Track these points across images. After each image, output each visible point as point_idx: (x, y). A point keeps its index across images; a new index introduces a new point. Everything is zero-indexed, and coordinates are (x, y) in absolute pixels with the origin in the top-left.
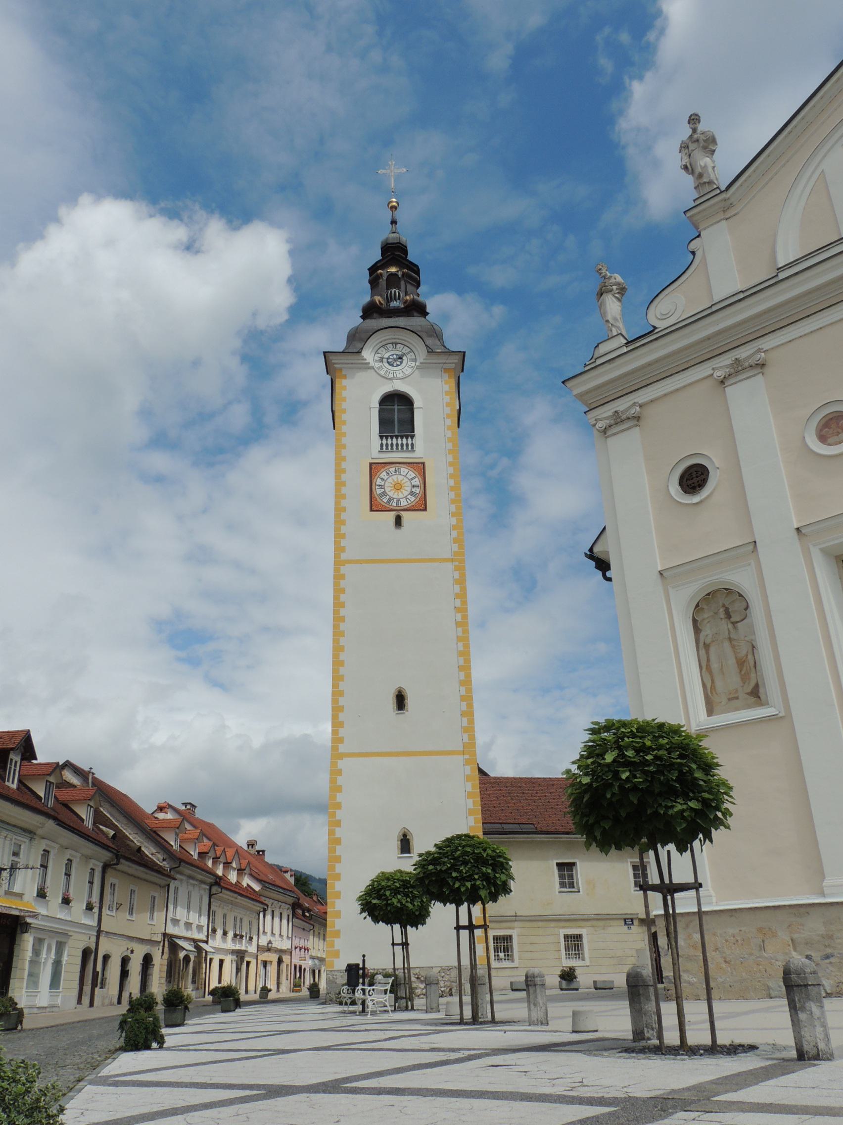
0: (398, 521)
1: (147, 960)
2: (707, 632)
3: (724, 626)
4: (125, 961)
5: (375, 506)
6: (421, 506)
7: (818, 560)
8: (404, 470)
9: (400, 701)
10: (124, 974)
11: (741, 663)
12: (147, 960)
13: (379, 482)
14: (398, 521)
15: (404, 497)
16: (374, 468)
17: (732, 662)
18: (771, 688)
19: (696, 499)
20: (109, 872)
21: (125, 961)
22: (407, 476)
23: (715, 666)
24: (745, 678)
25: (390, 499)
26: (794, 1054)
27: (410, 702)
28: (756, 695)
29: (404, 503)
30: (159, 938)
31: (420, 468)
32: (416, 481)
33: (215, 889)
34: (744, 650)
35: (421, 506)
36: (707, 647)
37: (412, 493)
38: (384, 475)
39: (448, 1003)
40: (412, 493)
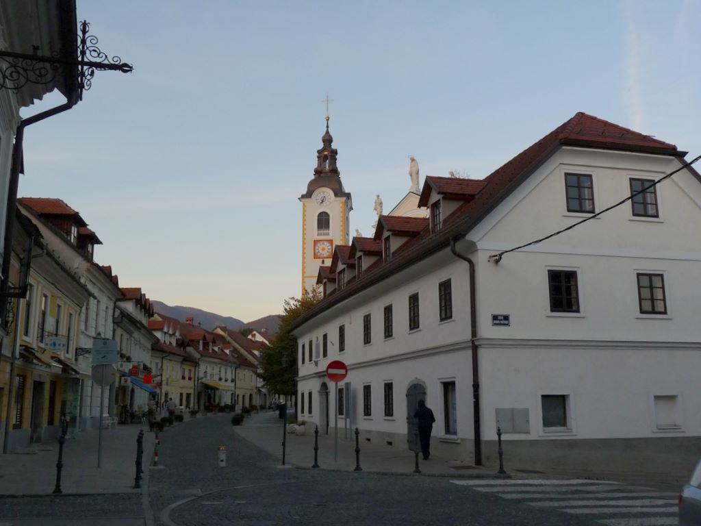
4: (244, 396)
8: (325, 243)
12: (251, 395)
16: (316, 242)
29: (325, 255)
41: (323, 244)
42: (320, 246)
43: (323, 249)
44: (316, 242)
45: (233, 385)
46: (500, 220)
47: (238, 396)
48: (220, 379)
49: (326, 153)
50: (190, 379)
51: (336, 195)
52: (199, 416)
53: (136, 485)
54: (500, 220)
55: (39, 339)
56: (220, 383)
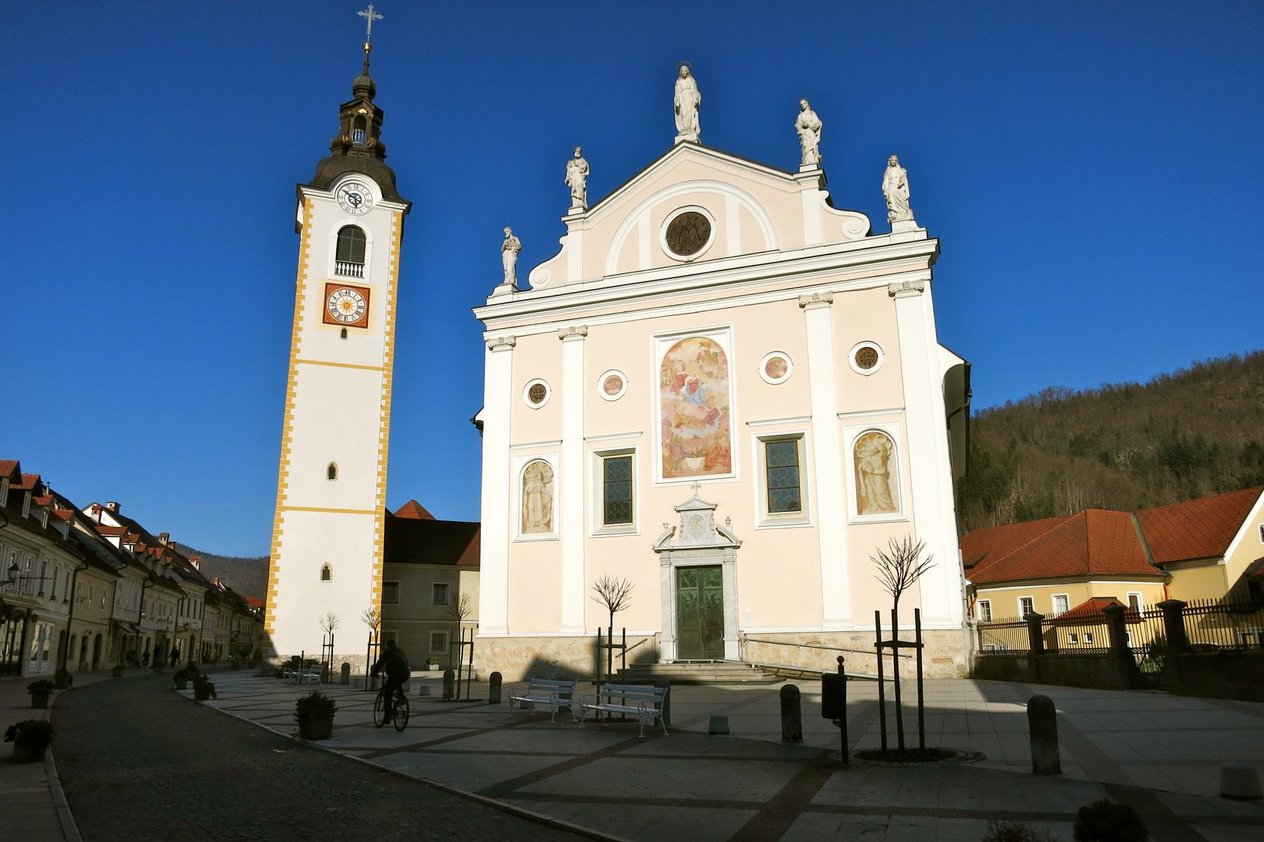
0: (344, 334)
1: (99, 637)
2: (530, 486)
3: (539, 484)
4: (85, 639)
5: (327, 319)
6: (363, 323)
7: (591, 455)
8: (353, 293)
9: (332, 472)
10: (84, 649)
11: (544, 507)
12: (99, 637)
13: (332, 300)
14: (344, 334)
15: (351, 315)
16: (330, 288)
17: (540, 505)
18: (555, 524)
19: (541, 404)
20: (79, 573)
21: (85, 639)
22: (355, 299)
23: (531, 506)
24: (544, 515)
25: (340, 315)
26: (1030, 769)
27: (339, 473)
28: (548, 525)
29: (350, 319)
30: (106, 622)
31: (366, 293)
32: (362, 304)
33: (148, 583)
34: (547, 500)
35: (363, 323)
36: (528, 494)
37: (357, 313)
38: (336, 295)
39: (598, 704)
40: (357, 313)
41: (347, 294)
42: (338, 299)
43: (347, 306)
44: (330, 288)
45: (65, 609)
46: (718, 758)
47: (74, 637)
48: (41, 594)
49: (362, 111)
50: (53, 598)
51: (385, 196)
52: (126, 674)
53: (445, 696)
54: (718, 758)
55: (1020, 641)
56: (40, 600)
